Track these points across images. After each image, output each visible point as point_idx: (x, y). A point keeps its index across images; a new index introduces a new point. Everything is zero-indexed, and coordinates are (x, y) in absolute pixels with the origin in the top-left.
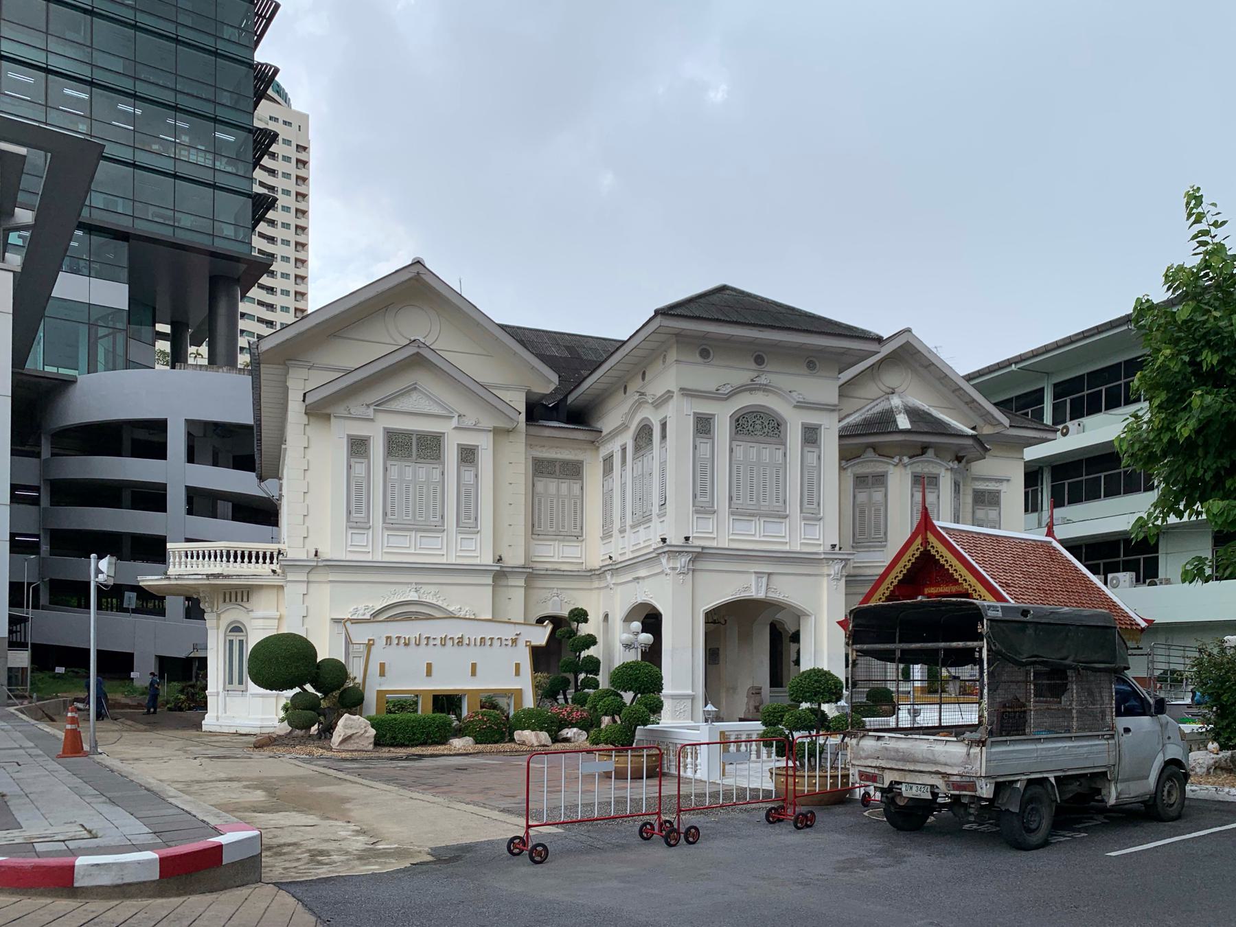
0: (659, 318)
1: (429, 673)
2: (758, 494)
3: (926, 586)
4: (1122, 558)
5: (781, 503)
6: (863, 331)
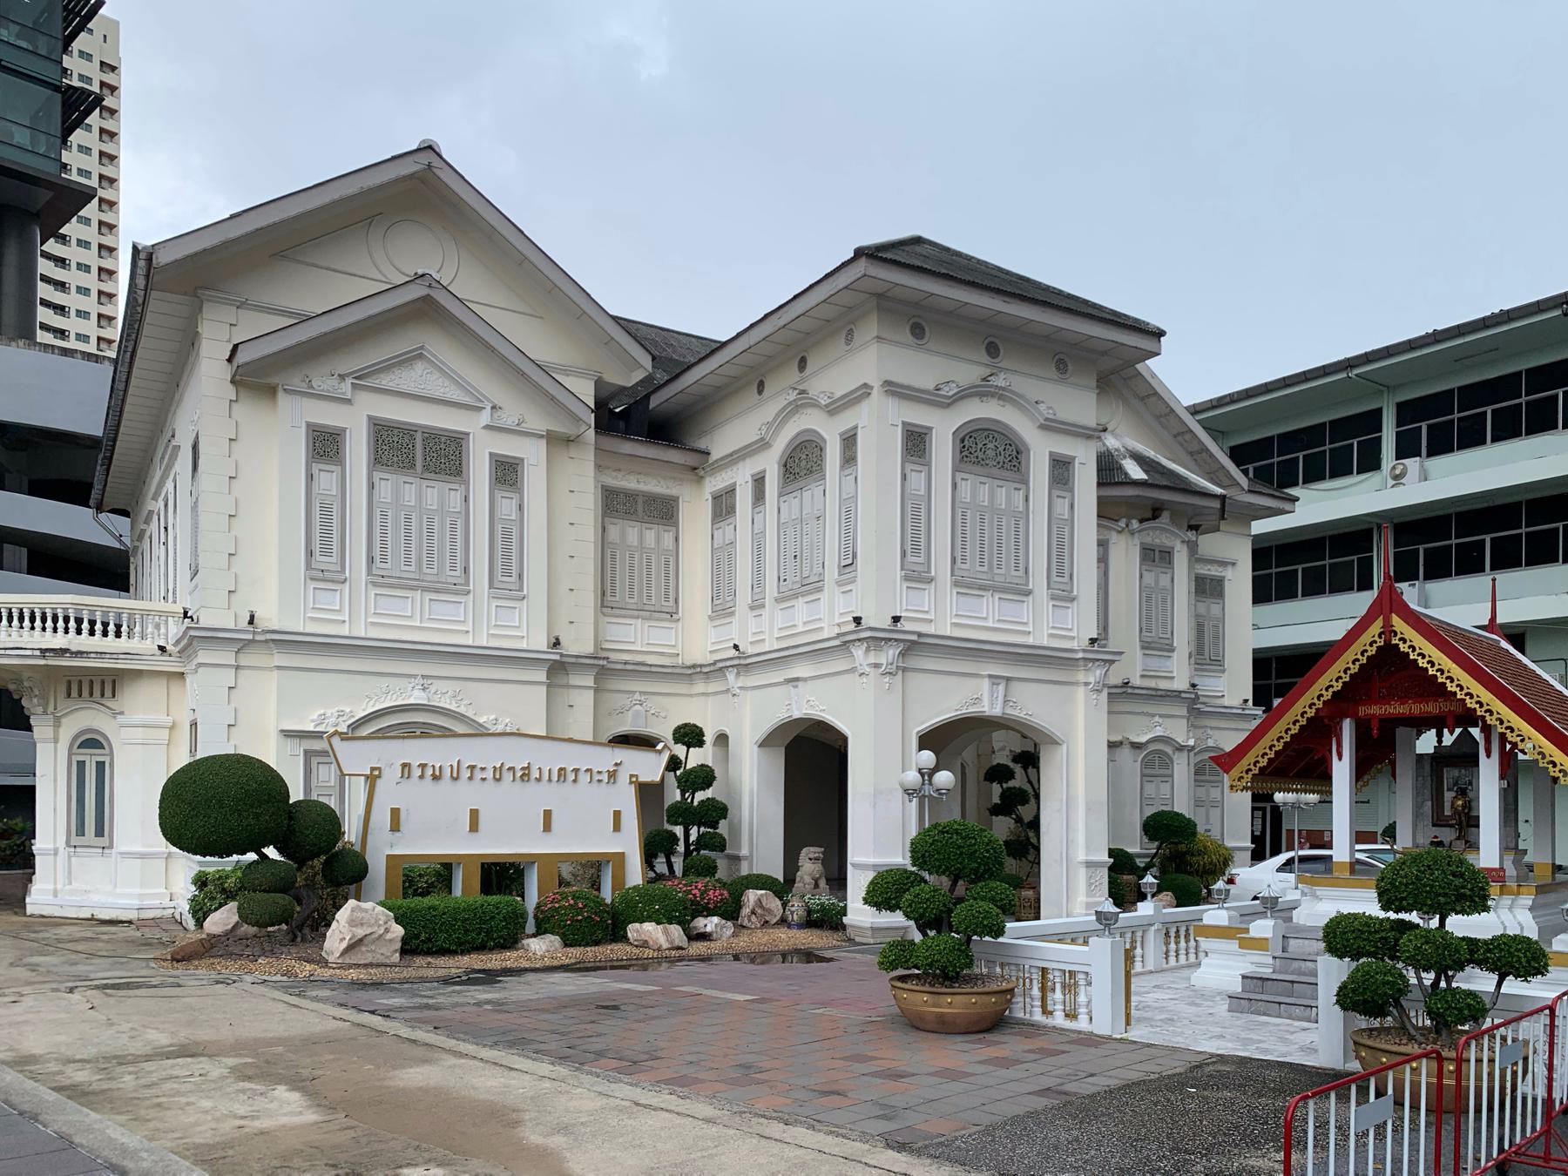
0: (863, 262)
1: (474, 826)
2: (991, 555)
4: (1273, 681)
5: (1021, 573)
6: (1136, 320)
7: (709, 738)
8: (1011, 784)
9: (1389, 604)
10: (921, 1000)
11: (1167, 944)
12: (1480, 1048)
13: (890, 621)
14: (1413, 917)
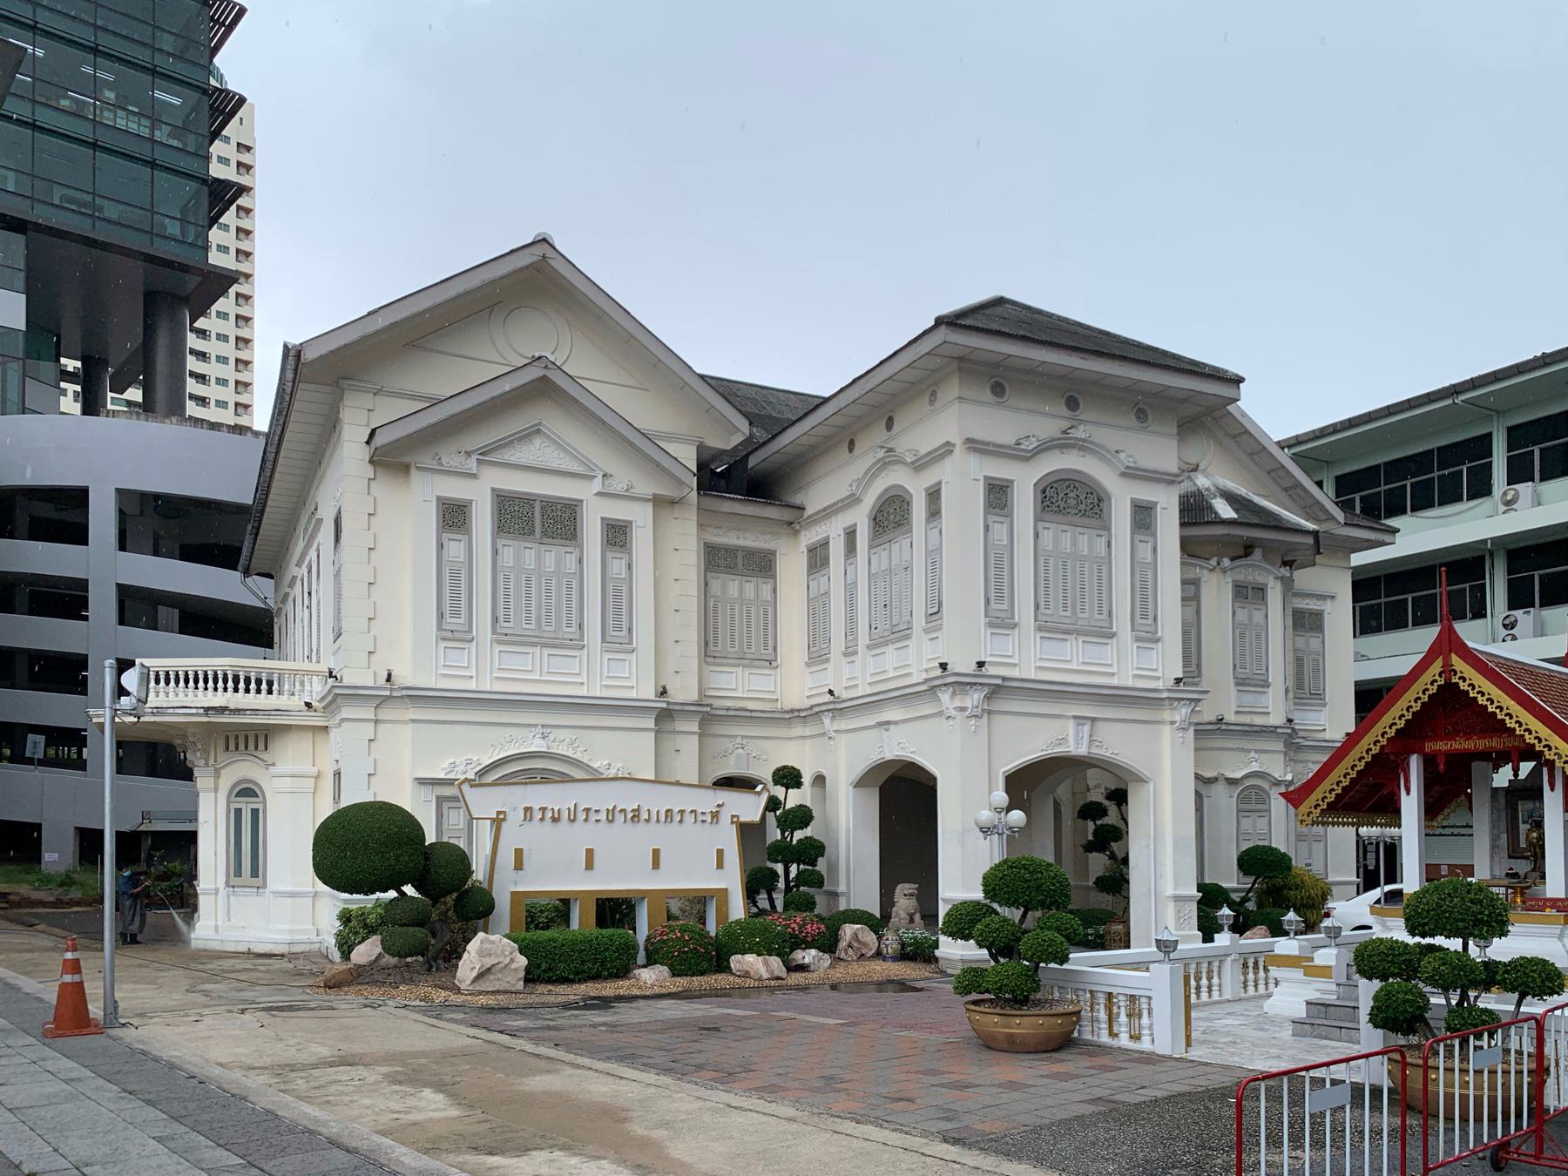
0: (943, 328)
1: (589, 865)
3: (1426, 738)
6: (1215, 368)
7: (807, 779)
9: (1448, 644)
10: (993, 1021)
11: (1245, 974)
12: (1449, 1054)
13: (974, 666)
14: (1439, 941)
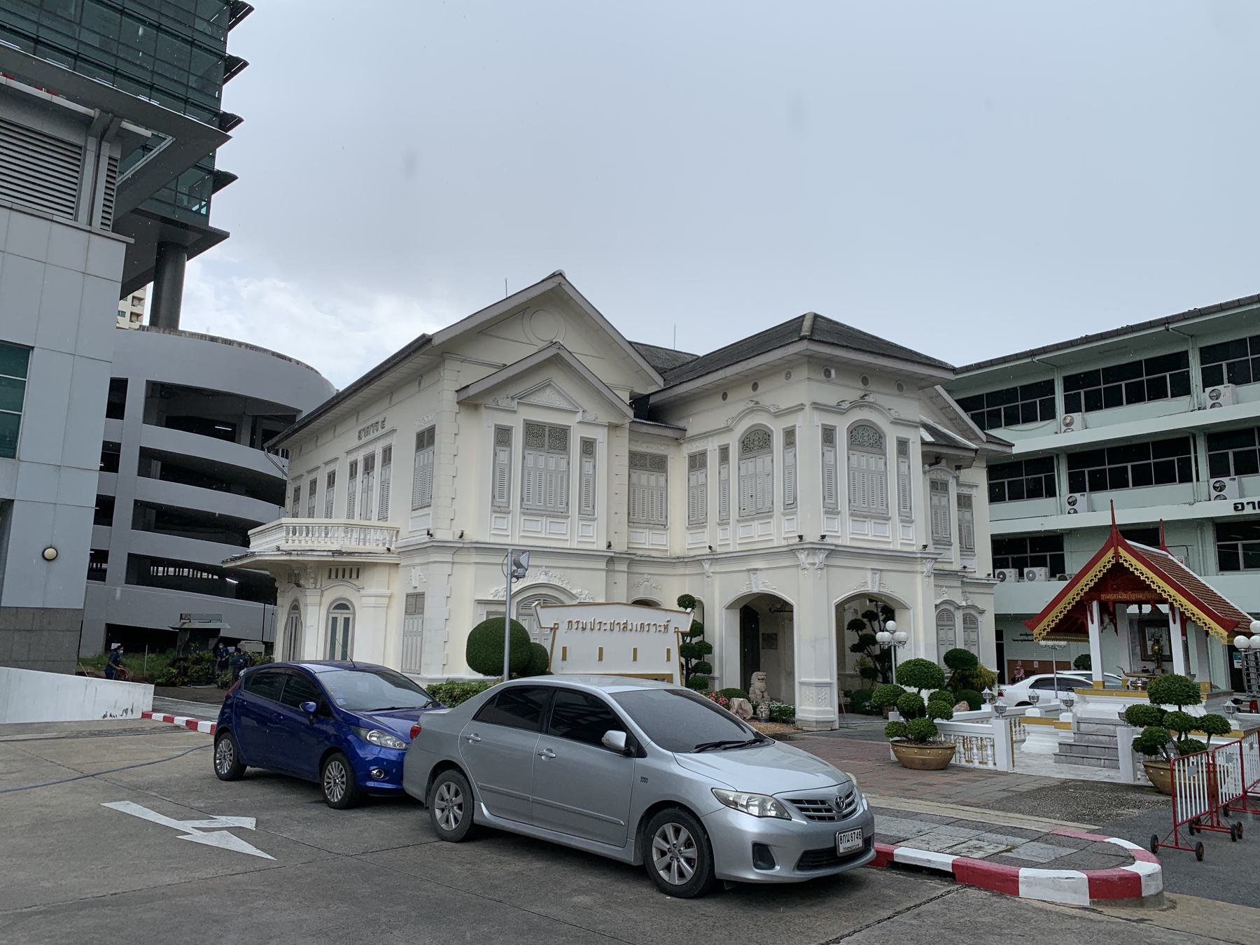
8: (864, 632)
